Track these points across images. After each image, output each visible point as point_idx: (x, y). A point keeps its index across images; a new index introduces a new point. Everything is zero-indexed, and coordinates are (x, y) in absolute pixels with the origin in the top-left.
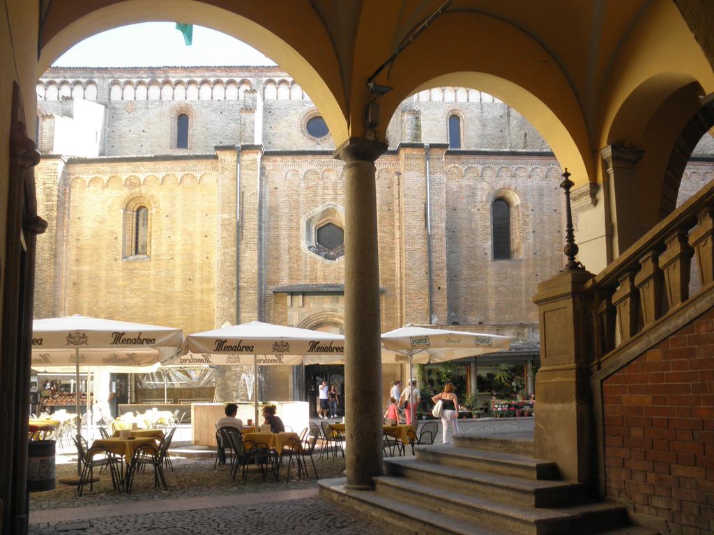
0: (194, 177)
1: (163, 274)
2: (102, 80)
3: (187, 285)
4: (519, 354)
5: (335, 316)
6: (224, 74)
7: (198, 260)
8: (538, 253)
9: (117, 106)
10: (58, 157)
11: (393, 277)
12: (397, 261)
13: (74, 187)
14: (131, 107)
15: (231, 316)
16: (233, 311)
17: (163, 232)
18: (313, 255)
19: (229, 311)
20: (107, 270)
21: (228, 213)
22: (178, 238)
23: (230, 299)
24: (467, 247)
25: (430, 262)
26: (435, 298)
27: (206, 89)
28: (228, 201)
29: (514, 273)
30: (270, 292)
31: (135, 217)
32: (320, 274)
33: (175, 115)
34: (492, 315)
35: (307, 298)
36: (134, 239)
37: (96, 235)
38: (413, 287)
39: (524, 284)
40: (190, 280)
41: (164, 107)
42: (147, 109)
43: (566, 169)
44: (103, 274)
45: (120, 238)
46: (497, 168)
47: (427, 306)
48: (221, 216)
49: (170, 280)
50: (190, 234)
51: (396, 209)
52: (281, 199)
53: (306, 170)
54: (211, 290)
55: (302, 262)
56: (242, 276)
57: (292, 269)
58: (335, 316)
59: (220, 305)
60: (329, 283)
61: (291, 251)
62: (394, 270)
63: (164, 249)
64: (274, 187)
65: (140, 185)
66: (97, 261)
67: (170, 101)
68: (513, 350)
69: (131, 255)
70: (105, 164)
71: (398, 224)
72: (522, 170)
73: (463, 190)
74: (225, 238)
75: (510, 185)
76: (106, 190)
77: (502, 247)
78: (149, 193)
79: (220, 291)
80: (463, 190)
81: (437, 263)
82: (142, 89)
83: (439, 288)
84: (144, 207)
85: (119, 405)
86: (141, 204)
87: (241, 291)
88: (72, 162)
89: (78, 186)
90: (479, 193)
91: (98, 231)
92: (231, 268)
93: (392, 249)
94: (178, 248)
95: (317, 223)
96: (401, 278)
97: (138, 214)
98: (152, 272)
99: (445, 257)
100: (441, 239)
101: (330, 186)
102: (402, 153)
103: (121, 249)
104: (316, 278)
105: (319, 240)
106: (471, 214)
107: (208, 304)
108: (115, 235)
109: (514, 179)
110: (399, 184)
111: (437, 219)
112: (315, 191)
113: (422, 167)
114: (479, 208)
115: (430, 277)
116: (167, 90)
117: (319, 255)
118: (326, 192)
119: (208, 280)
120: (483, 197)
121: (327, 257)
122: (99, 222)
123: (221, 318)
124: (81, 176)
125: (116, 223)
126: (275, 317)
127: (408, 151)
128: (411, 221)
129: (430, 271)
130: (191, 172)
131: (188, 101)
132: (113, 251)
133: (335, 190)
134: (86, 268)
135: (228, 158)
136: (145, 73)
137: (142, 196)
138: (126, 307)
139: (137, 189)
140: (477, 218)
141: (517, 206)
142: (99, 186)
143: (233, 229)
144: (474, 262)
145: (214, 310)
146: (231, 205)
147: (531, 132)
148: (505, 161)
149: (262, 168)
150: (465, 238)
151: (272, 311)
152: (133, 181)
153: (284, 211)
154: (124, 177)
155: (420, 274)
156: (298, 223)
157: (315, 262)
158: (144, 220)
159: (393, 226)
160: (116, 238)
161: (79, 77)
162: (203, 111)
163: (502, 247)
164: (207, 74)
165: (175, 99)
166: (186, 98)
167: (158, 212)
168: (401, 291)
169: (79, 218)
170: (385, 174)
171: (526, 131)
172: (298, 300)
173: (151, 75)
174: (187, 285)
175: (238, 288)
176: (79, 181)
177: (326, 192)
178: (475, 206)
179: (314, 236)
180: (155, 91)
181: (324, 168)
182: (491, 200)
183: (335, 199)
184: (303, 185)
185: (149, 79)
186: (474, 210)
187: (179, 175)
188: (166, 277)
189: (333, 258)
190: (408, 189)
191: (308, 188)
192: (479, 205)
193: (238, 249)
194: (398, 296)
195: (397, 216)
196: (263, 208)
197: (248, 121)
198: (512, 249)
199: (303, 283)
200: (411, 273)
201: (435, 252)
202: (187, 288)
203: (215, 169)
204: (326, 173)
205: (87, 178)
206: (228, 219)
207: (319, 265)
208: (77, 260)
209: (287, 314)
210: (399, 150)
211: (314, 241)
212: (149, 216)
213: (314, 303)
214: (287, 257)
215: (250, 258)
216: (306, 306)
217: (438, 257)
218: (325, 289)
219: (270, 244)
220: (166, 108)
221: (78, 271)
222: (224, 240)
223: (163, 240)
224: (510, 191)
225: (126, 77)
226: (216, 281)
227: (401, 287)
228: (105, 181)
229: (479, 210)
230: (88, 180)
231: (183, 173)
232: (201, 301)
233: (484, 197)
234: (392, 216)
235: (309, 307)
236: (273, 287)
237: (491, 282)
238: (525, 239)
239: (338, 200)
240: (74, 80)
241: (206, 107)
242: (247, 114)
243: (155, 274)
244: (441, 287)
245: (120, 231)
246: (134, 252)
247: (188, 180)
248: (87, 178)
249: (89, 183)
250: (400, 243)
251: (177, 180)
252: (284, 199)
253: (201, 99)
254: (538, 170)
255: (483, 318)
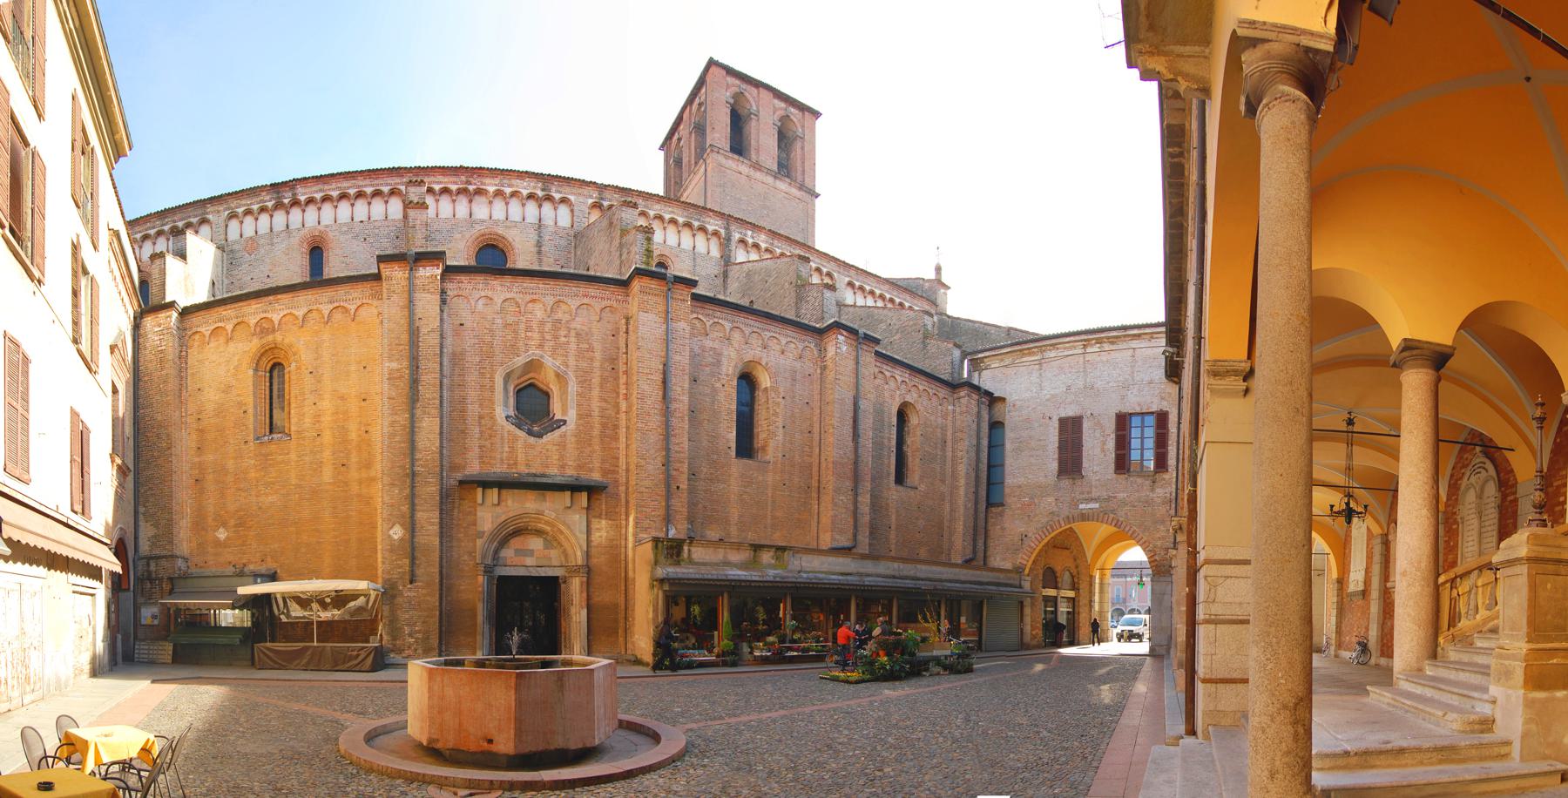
0: (346, 310)
1: (307, 458)
2: (218, 215)
3: (339, 473)
4: (785, 585)
5: (539, 520)
6: (367, 182)
7: (353, 436)
8: (787, 455)
9: (236, 247)
10: (172, 305)
11: (617, 469)
12: (622, 446)
13: (192, 347)
14: (252, 244)
15: (403, 516)
16: (405, 508)
17: (306, 396)
18: (512, 428)
19: (399, 510)
20: (236, 458)
21: (398, 359)
22: (326, 404)
23: (400, 490)
24: (708, 435)
25: (667, 449)
26: (673, 502)
27: (344, 207)
28: (397, 342)
29: (761, 478)
30: (453, 482)
31: (267, 379)
32: (521, 457)
33: (306, 249)
34: (734, 531)
35: (504, 492)
36: (268, 412)
37: (220, 411)
38: (647, 483)
39: (770, 495)
40: (343, 465)
41: (292, 240)
42: (272, 245)
43: (938, 269)
44: (230, 464)
45: (251, 411)
46: (747, 331)
47: (662, 512)
48: (387, 364)
49: (318, 467)
50: (342, 398)
51: (622, 368)
52: (469, 342)
53: (503, 298)
54: (373, 479)
55: (497, 440)
56: (418, 456)
57: (484, 449)
58: (539, 520)
59: (387, 499)
60: (534, 471)
61: (483, 421)
62: (618, 459)
63: (308, 420)
64: (459, 322)
65: (274, 331)
66: (222, 446)
67: (299, 230)
68: (778, 579)
69: (265, 435)
70: (228, 306)
71: (625, 391)
72: (775, 341)
73: (707, 354)
74: (394, 399)
75: (761, 358)
76: (231, 344)
77: (746, 446)
78: (287, 341)
79: (386, 480)
80: (707, 354)
81: (676, 452)
82: (264, 218)
83: (678, 488)
84: (280, 364)
85: (255, 645)
86: (275, 361)
87: (417, 479)
88: (186, 312)
89: (196, 344)
90: (725, 361)
91: (223, 404)
92: (403, 445)
93: (616, 427)
94: (327, 419)
95: (517, 382)
96: (627, 470)
97: (273, 369)
98: (293, 456)
99: (686, 444)
100: (682, 418)
101: (535, 325)
102: (636, 285)
103: (251, 427)
104: (516, 464)
105: (517, 409)
106: (714, 390)
107: (367, 500)
108: (244, 408)
109: (765, 350)
110: (627, 332)
111: (679, 389)
112: (516, 332)
113: (662, 308)
114: (724, 382)
115: (668, 470)
116: (296, 213)
117: (519, 428)
118: (529, 334)
119: (368, 465)
120: (729, 368)
121: (530, 433)
122: (223, 392)
123: (389, 520)
124: (199, 329)
125: (246, 389)
126: (460, 520)
127: (646, 282)
128: (646, 387)
129: (666, 464)
130: (342, 304)
131: (321, 228)
132: (242, 431)
133: (541, 332)
134: (209, 457)
135: (396, 274)
136: (268, 194)
137: (276, 347)
138: (260, 508)
139: (270, 338)
140: (721, 397)
141: (766, 388)
142: (222, 340)
143: (403, 384)
144: (715, 457)
145: (376, 510)
146: (401, 347)
147: (761, 301)
148: (757, 324)
149: (443, 292)
150: (706, 422)
151: (456, 511)
152: (264, 325)
153: (472, 359)
154: (253, 321)
155: (654, 466)
156: (492, 380)
157: (515, 439)
158: (279, 385)
159: (618, 394)
160: (245, 412)
161: (190, 217)
162: (342, 238)
163: (746, 446)
164: (345, 184)
165: (306, 226)
166: (319, 223)
167: (298, 368)
168: (627, 489)
169: (199, 389)
170: (609, 315)
171: (753, 298)
172: (493, 494)
173: (275, 196)
174: (339, 473)
175: (414, 474)
176: (197, 337)
177: (529, 334)
178: (719, 379)
179: (512, 401)
180: (280, 217)
181: (528, 298)
182: (737, 375)
183: (541, 346)
184: (499, 321)
185: (273, 202)
186: (718, 385)
187: (326, 309)
188: (311, 463)
189: (540, 436)
190: (643, 338)
191: (506, 325)
192: (724, 379)
193: (413, 416)
194: (623, 495)
195: (623, 379)
196: (445, 355)
197: (418, 222)
198: (755, 446)
199: (499, 470)
200: (643, 462)
201: (675, 436)
202: (340, 477)
203: (378, 296)
204: (530, 305)
205: (206, 330)
206: (398, 370)
207: (520, 444)
208: (199, 448)
209: (475, 515)
210: (631, 278)
211: (512, 409)
212: (287, 376)
213: (513, 502)
214: (477, 430)
215: (429, 427)
216: (503, 504)
217: (678, 444)
218: (531, 480)
219: (453, 411)
220: (295, 240)
221: (200, 463)
222: (391, 401)
223: (306, 409)
224: (760, 368)
225: (244, 205)
226: (379, 467)
227: (627, 483)
228: (229, 331)
229: (723, 385)
230: (207, 334)
231: (331, 307)
232: (359, 495)
233: (730, 369)
234: (617, 379)
235: (507, 506)
236: (459, 476)
237: (734, 486)
238: (772, 434)
239: (546, 348)
240: (183, 222)
241: (345, 233)
242: (418, 211)
243: (296, 459)
244: (681, 486)
245: (250, 400)
246: (268, 430)
247: (338, 316)
248: (206, 330)
249: (210, 337)
250: (628, 420)
251: (324, 318)
252: (473, 341)
253: (338, 222)
254: (793, 346)
255: (723, 534)
